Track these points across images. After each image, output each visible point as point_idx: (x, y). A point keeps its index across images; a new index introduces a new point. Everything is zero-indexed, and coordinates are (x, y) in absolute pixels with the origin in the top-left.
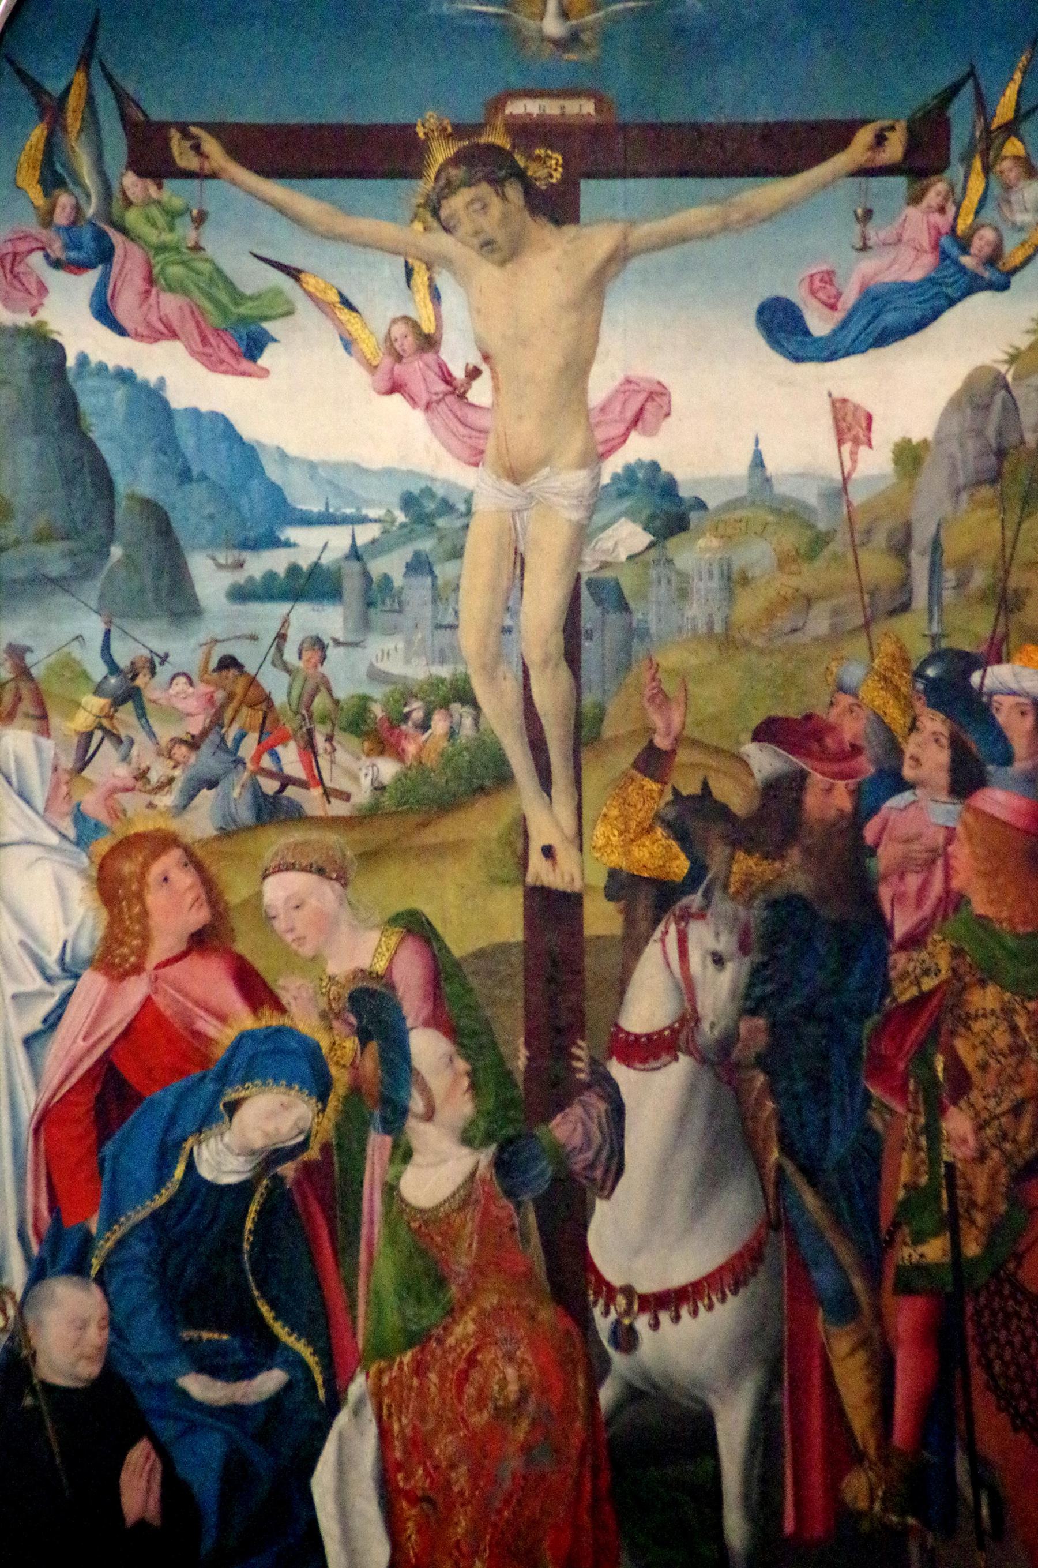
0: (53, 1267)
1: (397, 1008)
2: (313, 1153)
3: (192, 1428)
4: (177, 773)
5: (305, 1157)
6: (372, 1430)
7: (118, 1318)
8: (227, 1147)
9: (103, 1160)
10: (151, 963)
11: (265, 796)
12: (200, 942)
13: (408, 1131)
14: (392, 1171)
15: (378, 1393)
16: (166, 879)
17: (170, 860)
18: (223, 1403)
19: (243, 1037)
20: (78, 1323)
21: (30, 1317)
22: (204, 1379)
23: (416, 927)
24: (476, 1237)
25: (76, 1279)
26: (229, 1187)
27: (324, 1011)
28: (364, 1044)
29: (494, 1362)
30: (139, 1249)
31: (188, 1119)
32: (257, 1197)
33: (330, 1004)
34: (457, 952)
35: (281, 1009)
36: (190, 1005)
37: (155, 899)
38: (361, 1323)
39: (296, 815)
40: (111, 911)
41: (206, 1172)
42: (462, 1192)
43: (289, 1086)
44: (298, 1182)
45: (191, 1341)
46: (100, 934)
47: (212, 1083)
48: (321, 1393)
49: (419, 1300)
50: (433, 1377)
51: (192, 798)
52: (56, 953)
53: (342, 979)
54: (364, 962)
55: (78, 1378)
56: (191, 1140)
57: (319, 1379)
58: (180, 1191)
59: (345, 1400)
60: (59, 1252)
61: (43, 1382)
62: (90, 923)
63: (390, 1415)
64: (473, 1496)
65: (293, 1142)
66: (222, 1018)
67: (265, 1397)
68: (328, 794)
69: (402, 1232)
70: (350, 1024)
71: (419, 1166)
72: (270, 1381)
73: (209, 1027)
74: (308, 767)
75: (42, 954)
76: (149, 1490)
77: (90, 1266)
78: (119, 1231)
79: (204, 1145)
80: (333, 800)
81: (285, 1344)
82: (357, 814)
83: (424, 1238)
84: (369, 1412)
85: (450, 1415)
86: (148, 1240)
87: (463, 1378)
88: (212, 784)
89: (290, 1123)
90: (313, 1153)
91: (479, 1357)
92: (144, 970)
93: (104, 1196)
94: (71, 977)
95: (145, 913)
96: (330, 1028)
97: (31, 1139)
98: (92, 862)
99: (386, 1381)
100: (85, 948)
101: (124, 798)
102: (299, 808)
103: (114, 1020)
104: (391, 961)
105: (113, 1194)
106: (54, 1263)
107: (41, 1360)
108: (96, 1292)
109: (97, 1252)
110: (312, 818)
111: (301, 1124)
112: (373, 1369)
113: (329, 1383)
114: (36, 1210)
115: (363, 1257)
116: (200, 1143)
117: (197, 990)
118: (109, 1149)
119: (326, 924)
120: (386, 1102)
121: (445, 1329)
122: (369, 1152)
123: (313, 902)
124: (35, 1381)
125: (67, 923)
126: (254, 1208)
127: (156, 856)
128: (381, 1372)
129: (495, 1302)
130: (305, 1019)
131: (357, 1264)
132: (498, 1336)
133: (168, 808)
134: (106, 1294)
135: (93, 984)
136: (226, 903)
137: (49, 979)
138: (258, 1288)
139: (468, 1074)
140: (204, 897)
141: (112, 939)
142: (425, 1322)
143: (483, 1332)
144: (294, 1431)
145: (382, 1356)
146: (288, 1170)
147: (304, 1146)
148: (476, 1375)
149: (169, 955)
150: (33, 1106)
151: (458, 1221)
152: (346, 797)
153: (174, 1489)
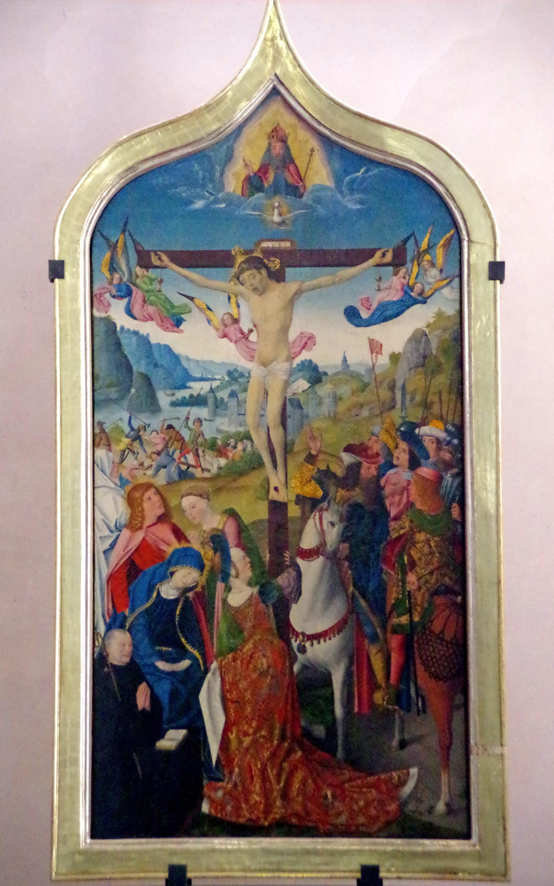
2: (199, 589)
6: (219, 679)
8: (170, 586)
15: (221, 668)
41: (163, 595)
44: (194, 599)
72: (185, 664)
78: (135, 614)
84: (218, 673)
99: (223, 663)
108: (127, 633)
112: (219, 659)
113: (205, 663)
115: (215, 622)
116: (161, 585)
118: (131, 588)
128: (221, 661)
138: (181, 632)
144: (193, 680)
146: (190, 595)
153: (154, 698)
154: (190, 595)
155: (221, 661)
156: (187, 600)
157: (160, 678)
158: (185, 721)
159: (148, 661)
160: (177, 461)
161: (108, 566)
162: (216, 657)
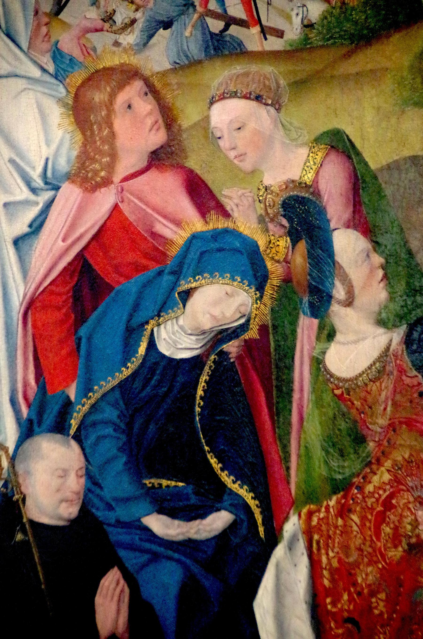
0: (39, 426)
1: (322, 211)
2: (253, 333)
3: (155, 557)
4: (138, 15)
5: (246, 336)
7: (94, 470)
8: (181, 327)
9: (80, 339)
10: (117, 178)
11: (212, 34)
12: (158, 159)
13: (332, 314)
14: (320, 347)
15: (308, 533)
16: (129, 107)
17: (133, 91)
18: (180, 538)
19: (194, 237)
20: (60, 473)
21: (20, 468)
22: (164, 518)
23: (338, 144)
24: (390, 403)
26: (183, 360)
27: (261, 215)
28: (294, 243)
29: (406, 506)
31: (149, 306)
32: (207, 369)
33: (266, 209)
34: (373, 166)
35: (226, 215)
36: (150, 211)
37: (121, 124)
38: (293, 472)
39: (239, 51)
40: (83, 133)
41: (164, 349)
42: (378, 365)
43: (233, 279)
44: (239, 357)
45: (153, 487)
46: (75, 153)
47: (169, 275)
48: (261, 529)
49: (342, 454)
50: (355, 517)
51: (151, 36)
52: (39, 169)
53: (276, 189)
54: (295, 173)
55: (60, 518)
56: (152, 322)
58: (142, 365)
59: (282, 537)
60: (43, 416)
61: (32, 522)
62: (67, 144)
63: (319, 549)
64: (390, 618)
65: (236, 324)
66: (178, 223)
67: (216, 533)
68: (265, 32)
69: (328, 398)
70: (283, 226)
71: (339, 343)
72: (219, 521)
73: (165, 229)
74: (249, 11)
75: (28, 169)
76: (118, 611)
77: (70, 425)
78: (94, 397)
79: (162, 326)
80: (268, 36)
81: (230, 489)
82: (289, 48)
83: (346, 400)
84: (301, 546)
85: (370, 550)
86: (115, 405)
87: (381, 519)
88: (167, 25)
90: (253, 333)
91: (394, 501)
92: (112, 182)
93: (81, 371)
94: (53, 189)
95: (113, 135)
96: (267, 230)
97: (20, 322)
98: (68, 91)
99: (315, 521)
100: (63, 165)
101: (94, 37)
102: (240, 44)
103: (88, 225)
104: (317, 174)
105: (88, 370)
106: (40, 424)
107: (29, 502)
108: (73, 443)
109: (75, 414)
110: (252, 52)
111: (243, 309)
112: (304, 511)
113: (268, 521)
114: (26, 385)
116: (159, 325)
117: (156, 200)
118: (83, 331)
119: (263, 143)
120: (313, 290)
121: (364, 478)
122: (299, 330)
123: (252, 125)
124: (25, 520)
125: (48, 143)
126: (204, 377)
127: (121, 86)
128: (310, 514)
129: (407, 456)
130: (246, 222)
131: (290, 424)
132: (410, 484)
133: (131, 47)
134: (83, 449)
135: (70, 195)
136: (180, 126)
137: (34, 191)
139: (383, 267)
140: (161, 121)
141: (85, 157)
142: (348, 472)
143: (397, 481)
146: (232, 348)
147: (244, 327)
148: (392, 517)
149: (132, 171)
150: (21, 298)
151: (374, 388)
152: (280, 34)
153: (139, 608)
154: (232, 348)
155: (310, 514)
156: (222, 354)
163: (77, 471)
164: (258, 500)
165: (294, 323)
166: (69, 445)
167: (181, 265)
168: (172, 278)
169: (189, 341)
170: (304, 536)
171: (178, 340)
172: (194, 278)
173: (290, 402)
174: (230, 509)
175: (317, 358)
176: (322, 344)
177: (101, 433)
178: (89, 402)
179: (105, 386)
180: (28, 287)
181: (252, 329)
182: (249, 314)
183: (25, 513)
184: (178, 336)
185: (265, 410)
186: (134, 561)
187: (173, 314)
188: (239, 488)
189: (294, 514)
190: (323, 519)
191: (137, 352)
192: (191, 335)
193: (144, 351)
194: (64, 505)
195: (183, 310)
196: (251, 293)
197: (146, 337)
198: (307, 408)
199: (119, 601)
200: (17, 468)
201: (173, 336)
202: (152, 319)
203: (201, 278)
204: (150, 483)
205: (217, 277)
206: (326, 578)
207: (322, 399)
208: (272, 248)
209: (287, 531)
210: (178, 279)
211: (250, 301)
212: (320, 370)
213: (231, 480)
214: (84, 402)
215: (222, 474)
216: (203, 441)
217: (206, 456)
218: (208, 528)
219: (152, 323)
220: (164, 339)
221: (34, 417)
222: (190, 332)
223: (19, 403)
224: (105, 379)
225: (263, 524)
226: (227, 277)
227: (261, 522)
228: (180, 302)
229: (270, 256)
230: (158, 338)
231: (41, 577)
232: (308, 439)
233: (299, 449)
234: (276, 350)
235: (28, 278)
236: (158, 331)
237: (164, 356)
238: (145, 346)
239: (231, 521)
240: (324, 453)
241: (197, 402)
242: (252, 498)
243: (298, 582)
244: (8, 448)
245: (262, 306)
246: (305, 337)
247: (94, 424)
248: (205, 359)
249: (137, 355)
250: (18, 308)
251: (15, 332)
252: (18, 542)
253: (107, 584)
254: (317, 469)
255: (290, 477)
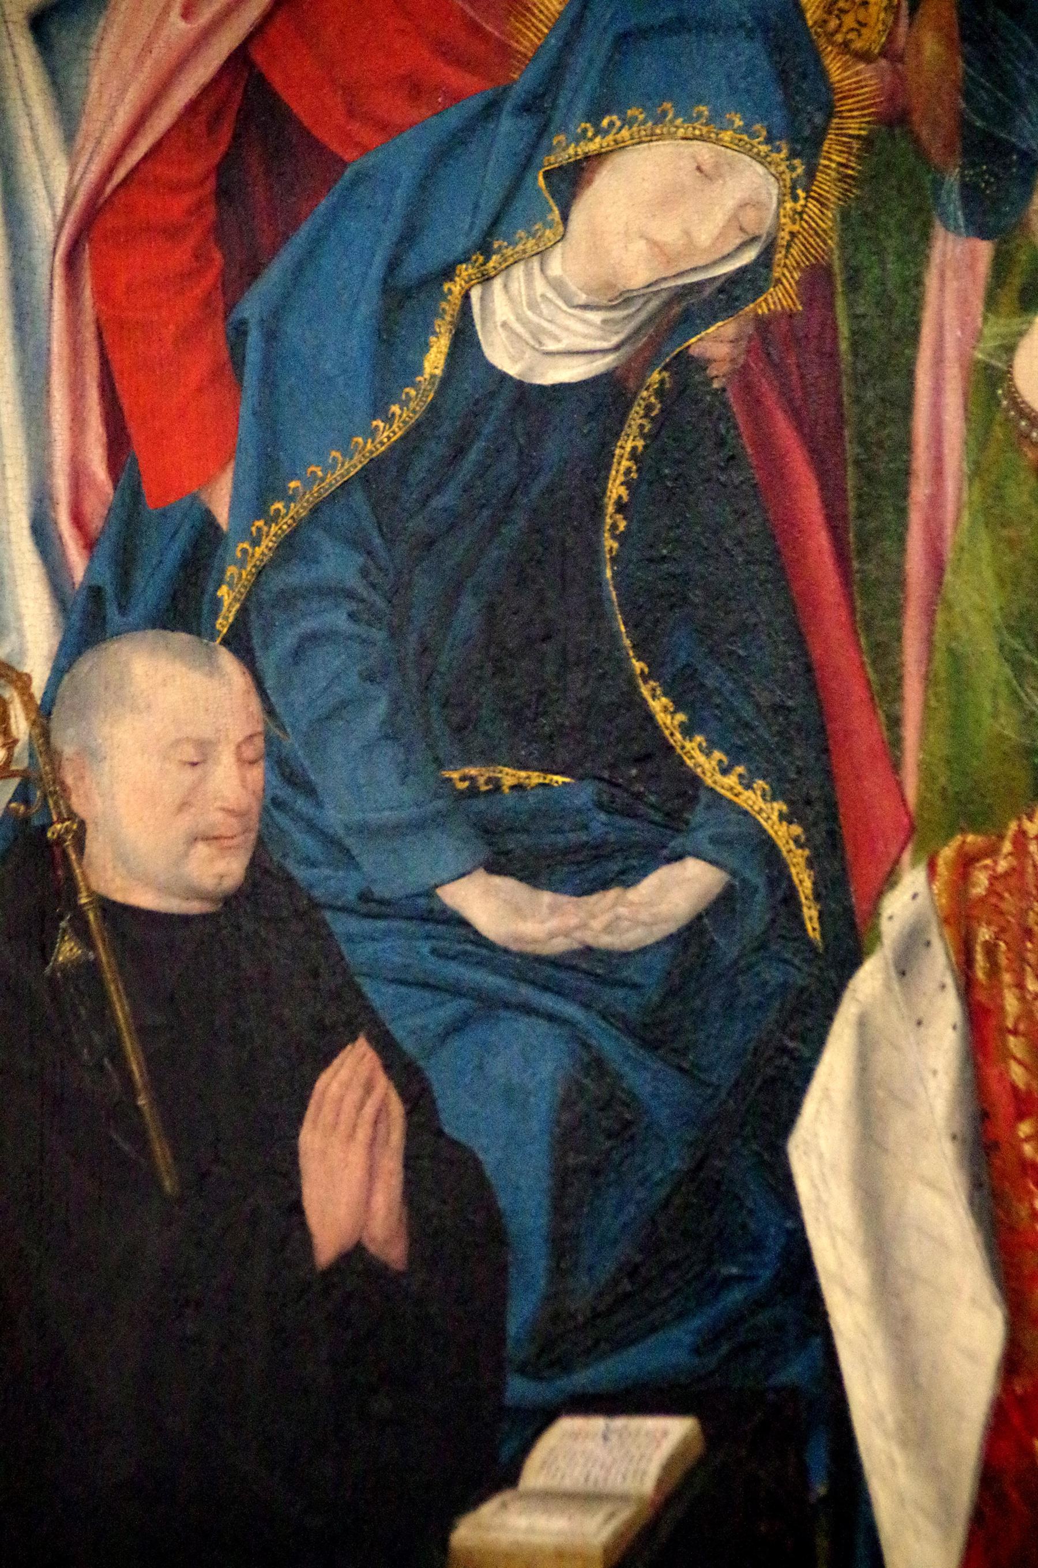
2: (779, 297)
6: (946, 1011)
7: (292, 743)
8: (557, 286)
9: (240, 330)
14: (996, 328)
15: (960, 918)
18: (559, 946)
20: (190, 753)
25: (181, 638)
30: (337, 564)
32: (636, 418)
38: (910, 734)
41: (503, 355)
43: (716, 119)
44: (742, 372)
48: (810, 913)
56: (465, 271)
57: (804, 881)
59: (878, 937)
60: (138, 576)
63: (994, 971)
67: (671, 928)
72: (676, 890)
76: (371, 1173)
77: (217, 602)
78: (288, 513)
79: (497, 284)
84: (938, 963)
89: (719, 218)
90: (779, 297)
97: (59, 270)
99: (981, 882)
105: (269, 421)
107: (96, 845)
108: (228, 662)
109: (231, 570)
111: (749, 219)
112: (947, 853)
113: (832, 886)
115: (915, 563)
116: (486, 279)
118: (251, 309)
126: (629, 443)
128: (966, 862)
131: (901, 583)
138: (641, 650)
144: (747, 1015)
145: (973, 824)
146: (717, 343)
153: (436, 1168)
154: (717, 343)
155: (966, 862)
156: (685, 366)
157: (490, 1005)
158: (668, 1350)
159: (391, 873)
160: (882, 337)
161: (69, 136)
162: (914, 832)
163: (239, 746)
164: (801, 823)
165: (917, 253)
166: (213, 669)
167: (555, 74)
168: (527, 123)
169: (579, 327)
170: (947, 931)
171: (546, 324)
172: (596, 125)
173: (902, 512)
174: (713, 856)
175: (987, 367)
176: (1002, 321)
177: (308, 625)
178: (274, 529)
179: (323, 480)
180: (80, 169)
181: (779, 281)
182: (769, 234)
183: (85, 878)
184: (545, 312)
185: (821, 540)
186: (418, 1021)
187: (531, 242)
188: (739, 788)
189: (914, 865)
190: (1006, 875)
191: (420, 370)
192: (585, 307)
193: (441, 363)
194: (202, 849)
195: (561, 229)
196: (778, 165)
197: (448, 318)
198: (955, 529)
199: (372, 1143)
200: (56, 740)
201: (529, 313)
202: (467, 260)
203: (618, 123)
204: (463, 779)
205: (670, 116)
206: (1015, 1058)
207: (1001, 498)
208: (842, 11)
209: (891, 918)
210: (543, 131)
211: (775, 191)
212: (999, 404)
213: (714, 763)
214: (259, 529)
215: (688, 745)
216: (627, 642)
217: (636, 688)
218: (644, 916)
219: (464, 274)
220: (504, 325)
221: (106, 578)
222: (583, 298)
223: (60, 537)
224: (321, 455)
225: (817, 897)
226: (700, 115)
227: (809, 892)
228: (551, 202)
229: (839, 38)
230: (484, 320)
231: (134, 1067)
232: (960, 628)
233: (930, 660)
234: (854, 346)
235: (79, 140)
236: (482, 299)
237: (504, 377)
238: (445, 350)
239: (717, 890)
240: (1007, 670)
241: (609, 521)
242: (782, 817)
243: (929, 1076)
244: (29, 677)
245: (813, 207)
246: (950, 297)
247: (287, 599)
248: (631, 384)
249: (419, 379)
250: (51, 237)
251: (44, 308)
252: (63, 968)
253: (335, 1087)
254: (987, 721)
255: (902, 751)
